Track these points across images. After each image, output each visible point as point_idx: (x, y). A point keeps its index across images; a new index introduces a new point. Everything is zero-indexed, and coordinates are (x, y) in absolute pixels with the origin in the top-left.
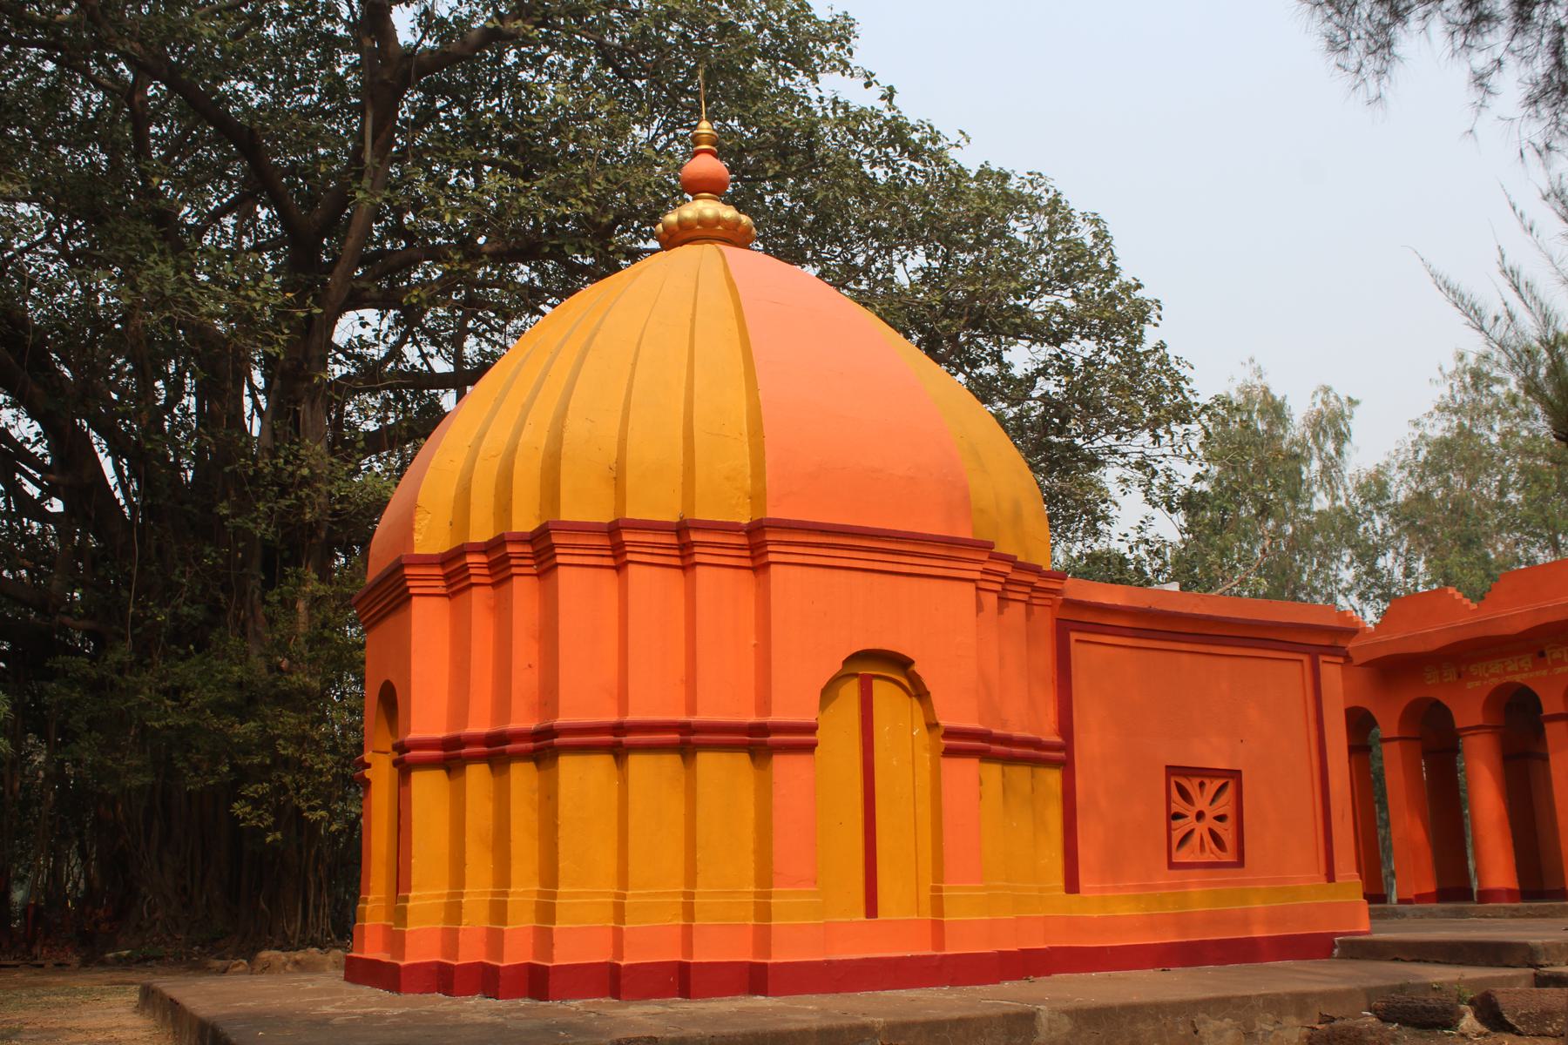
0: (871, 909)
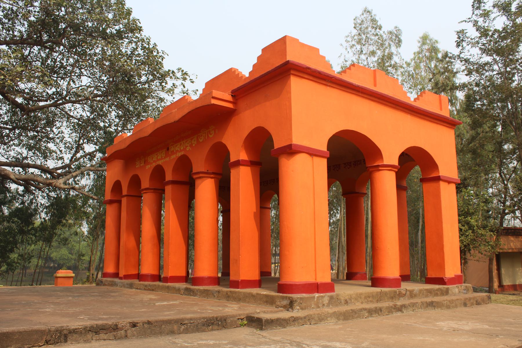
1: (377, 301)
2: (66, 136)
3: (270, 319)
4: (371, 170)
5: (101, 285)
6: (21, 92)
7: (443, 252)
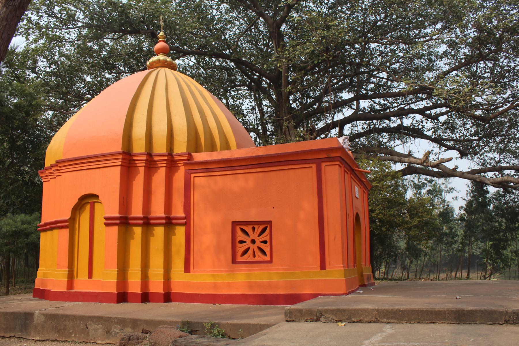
0: (90, 276)
6: (477, 106)
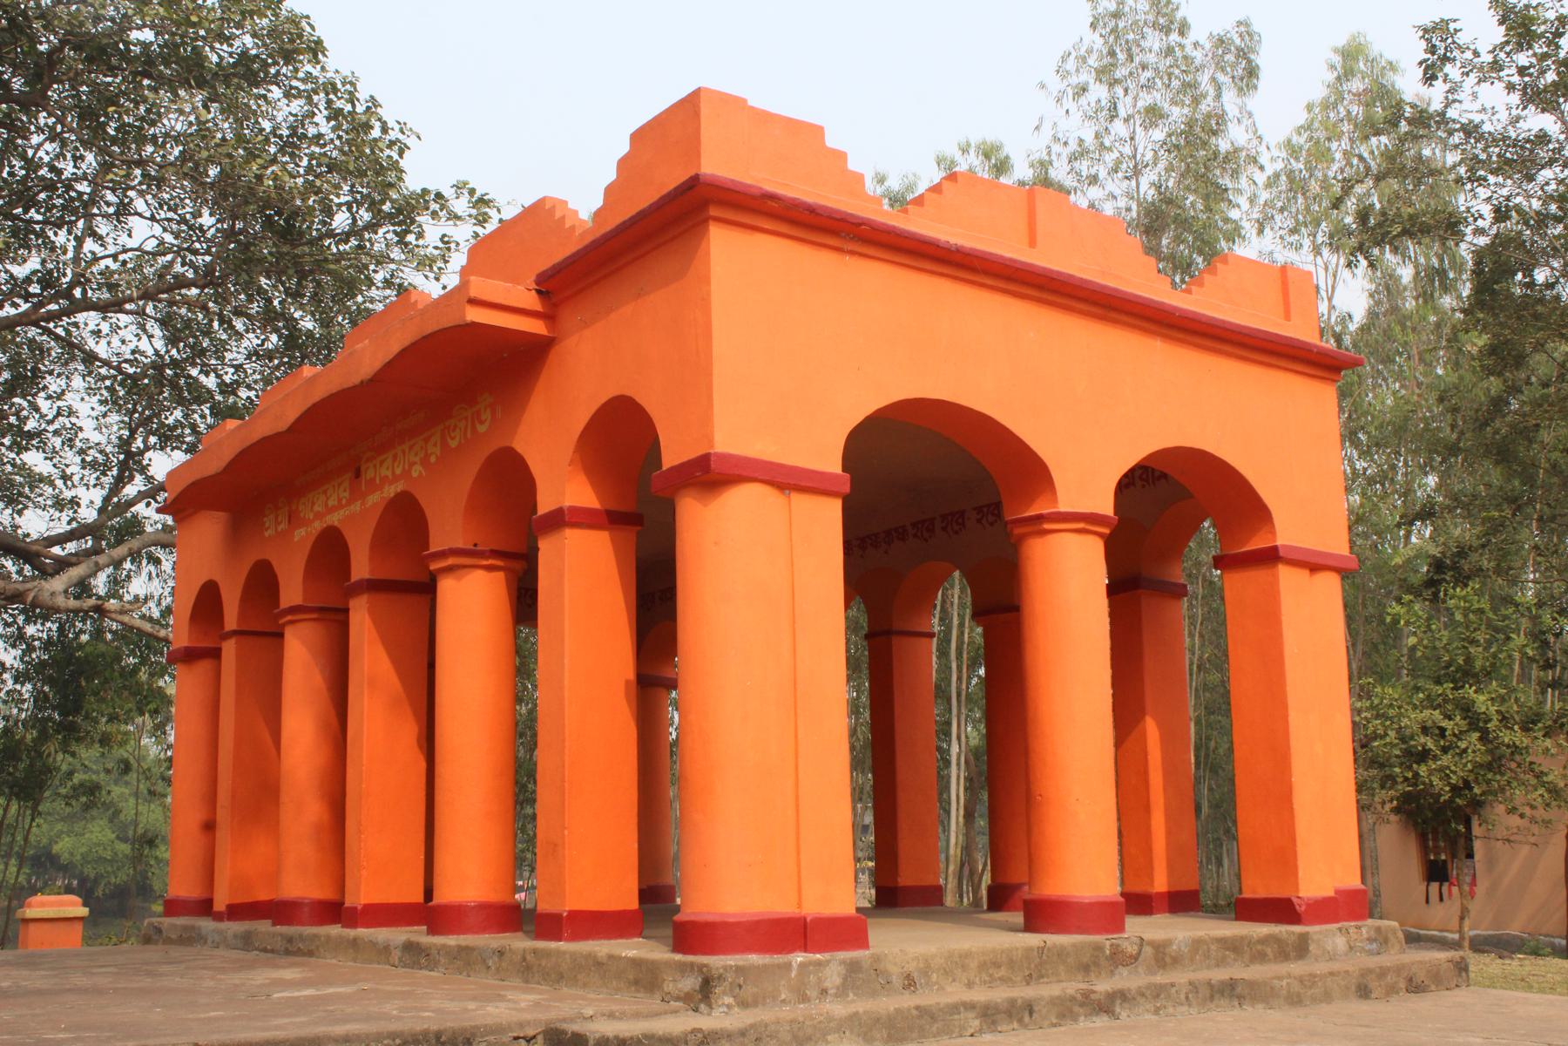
1: (1029, 979)
2: (88, 425)
3: (616, 1037)
4: (1018, 531)
5: (156, 943)
7: (1291, 810)
